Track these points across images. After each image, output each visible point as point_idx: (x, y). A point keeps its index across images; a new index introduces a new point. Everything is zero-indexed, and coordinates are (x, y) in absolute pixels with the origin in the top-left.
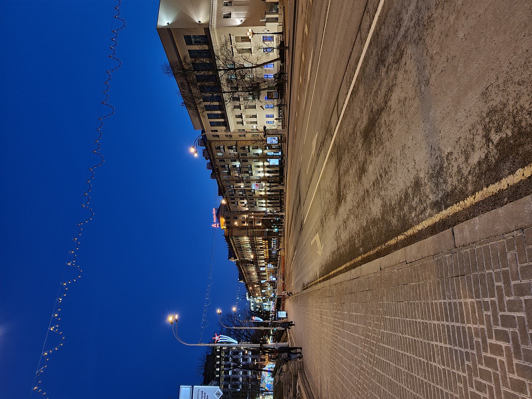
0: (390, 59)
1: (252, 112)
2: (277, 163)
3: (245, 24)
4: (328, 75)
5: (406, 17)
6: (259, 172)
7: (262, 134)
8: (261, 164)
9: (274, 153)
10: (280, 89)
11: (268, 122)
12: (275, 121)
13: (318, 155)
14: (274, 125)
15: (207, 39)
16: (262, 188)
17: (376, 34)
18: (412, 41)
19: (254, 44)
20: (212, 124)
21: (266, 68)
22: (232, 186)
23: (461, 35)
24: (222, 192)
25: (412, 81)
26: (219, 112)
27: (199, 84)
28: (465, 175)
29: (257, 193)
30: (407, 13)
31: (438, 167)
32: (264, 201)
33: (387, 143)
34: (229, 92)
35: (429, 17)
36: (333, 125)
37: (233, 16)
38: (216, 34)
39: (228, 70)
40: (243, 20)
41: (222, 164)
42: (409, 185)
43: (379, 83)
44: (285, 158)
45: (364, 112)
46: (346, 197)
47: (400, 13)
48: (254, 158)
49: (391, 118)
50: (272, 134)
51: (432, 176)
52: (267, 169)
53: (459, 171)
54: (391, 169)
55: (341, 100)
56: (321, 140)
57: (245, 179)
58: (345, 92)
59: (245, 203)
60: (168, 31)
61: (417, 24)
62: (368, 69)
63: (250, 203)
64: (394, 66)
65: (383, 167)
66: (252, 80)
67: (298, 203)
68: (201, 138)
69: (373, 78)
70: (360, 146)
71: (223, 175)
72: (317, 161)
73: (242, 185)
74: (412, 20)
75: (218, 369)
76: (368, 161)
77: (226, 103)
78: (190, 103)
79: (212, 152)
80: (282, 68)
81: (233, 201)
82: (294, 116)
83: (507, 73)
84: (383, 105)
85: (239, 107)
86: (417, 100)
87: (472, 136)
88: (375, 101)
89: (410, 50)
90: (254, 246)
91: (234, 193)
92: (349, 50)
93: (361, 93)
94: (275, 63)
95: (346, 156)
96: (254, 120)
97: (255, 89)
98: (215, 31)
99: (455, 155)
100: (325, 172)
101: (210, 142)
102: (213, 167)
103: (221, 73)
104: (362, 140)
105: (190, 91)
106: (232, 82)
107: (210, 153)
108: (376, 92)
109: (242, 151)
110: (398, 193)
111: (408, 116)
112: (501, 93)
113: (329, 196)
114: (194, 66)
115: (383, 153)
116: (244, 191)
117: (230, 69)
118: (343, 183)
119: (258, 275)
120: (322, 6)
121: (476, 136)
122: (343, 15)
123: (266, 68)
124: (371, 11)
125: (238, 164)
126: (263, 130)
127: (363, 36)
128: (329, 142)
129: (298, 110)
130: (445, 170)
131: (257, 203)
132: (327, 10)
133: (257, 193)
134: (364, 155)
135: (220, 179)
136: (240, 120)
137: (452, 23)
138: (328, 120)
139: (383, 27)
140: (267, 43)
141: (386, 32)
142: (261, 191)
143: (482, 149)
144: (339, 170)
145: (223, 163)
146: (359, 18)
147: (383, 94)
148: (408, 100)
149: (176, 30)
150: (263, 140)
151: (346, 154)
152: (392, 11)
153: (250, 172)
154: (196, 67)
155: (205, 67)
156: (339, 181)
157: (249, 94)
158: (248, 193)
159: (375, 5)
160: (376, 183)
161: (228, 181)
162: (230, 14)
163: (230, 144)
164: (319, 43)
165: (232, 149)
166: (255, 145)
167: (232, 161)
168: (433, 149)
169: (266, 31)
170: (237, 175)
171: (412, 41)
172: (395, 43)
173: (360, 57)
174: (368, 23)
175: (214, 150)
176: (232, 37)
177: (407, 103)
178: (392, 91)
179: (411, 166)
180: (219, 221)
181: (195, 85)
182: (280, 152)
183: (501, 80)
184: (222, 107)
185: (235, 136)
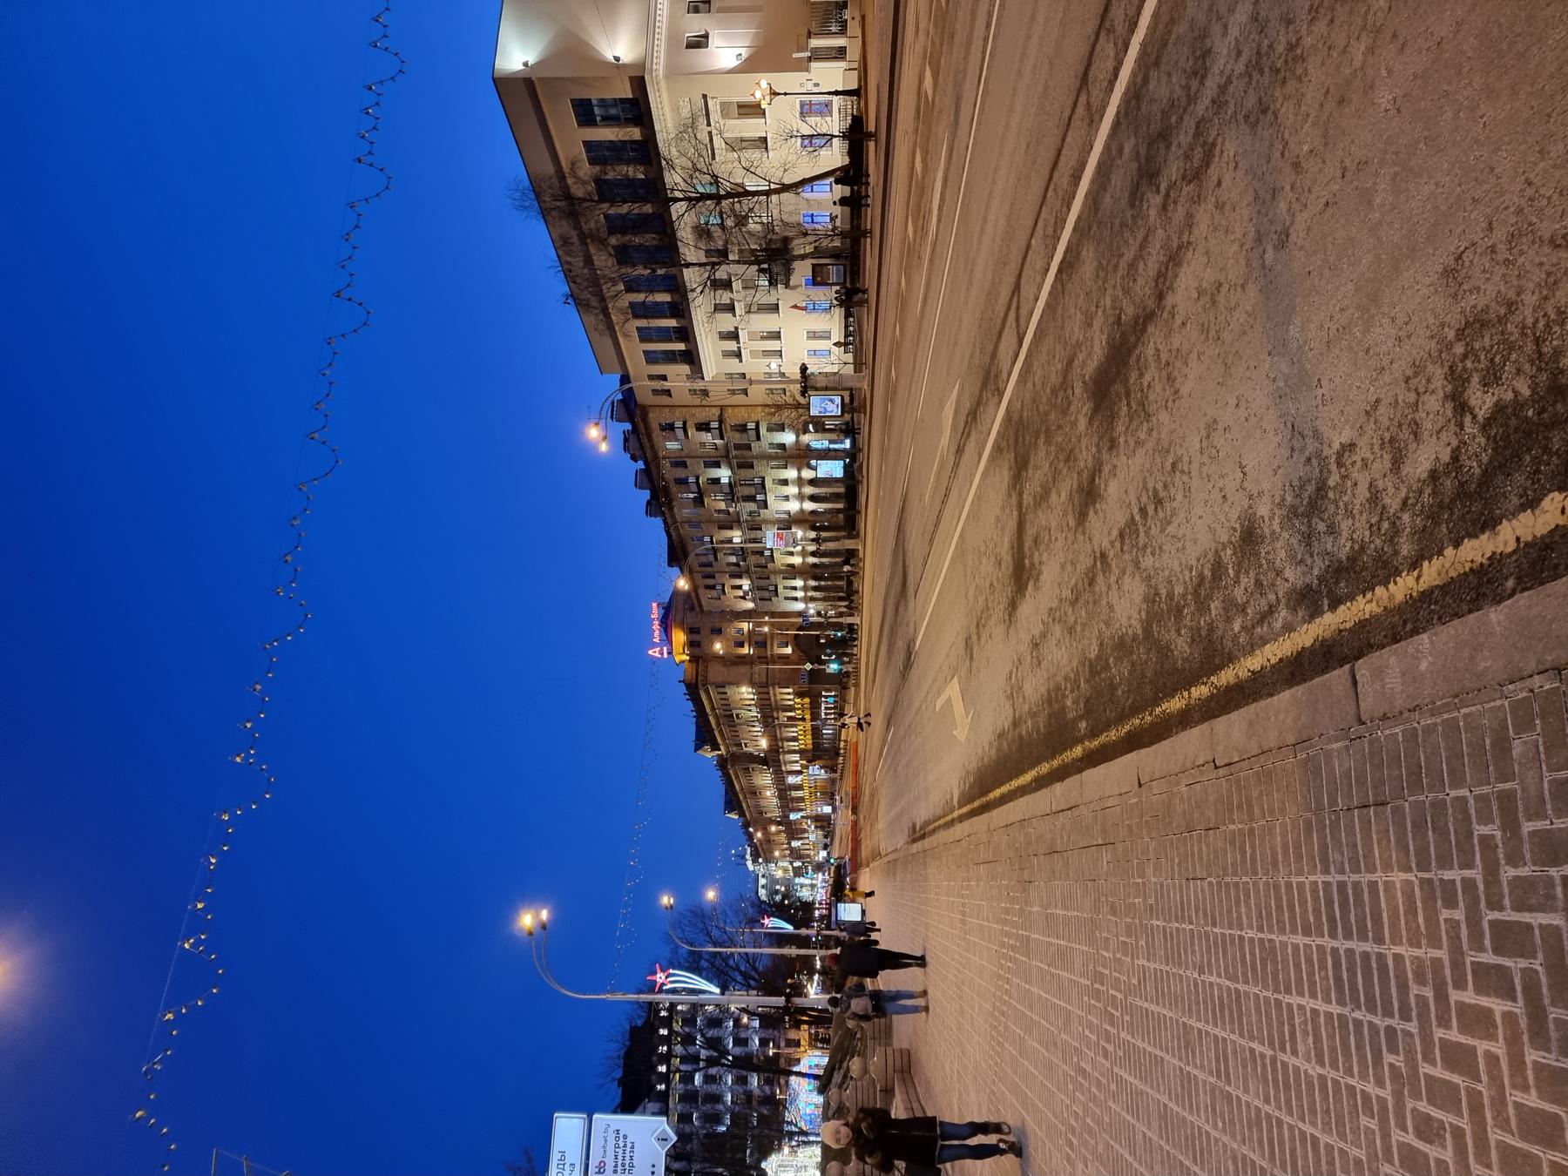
0: (1173, 170)
1: (767, 322)
4: (991, 217)
5: (1222, 48)
6: (787, 498)
8: (791, 474)
9: (831, 442)
10: (847, 268)
12: (835, 349)
13: (960, 451)
14: (831, 360)
15: (637, 110)
16: (795, 544)
20: (651, 358)
22: (707, 539)
23: (1384, 98)
26: (672, 323)
27: (613, 241)
28: (1392, 511)
29: (781, 560)
31: (1311, 488)
32: (799, 583)
33: (1164, 417)
34: (701, 265)
35: (1291, 47)
37: (715, 41)
39: (698, 200)
40: (745, 53)
41: (680, 473)
47: (1204, 35)
48: (770, 457)
50: (826, 389)
52: (809, 490)
54: (1173, 491)
55: (1027, 290)
58: (1039, 265)
59: (746, 588)
61: (1256, 65)
62: (1107, 199)
63: (761, 589)
65: (1150, 486)
66: (769, 228)
68: (620, 397)
69: (1123, 225)
70: (1082, 423)
71: (682, 506)
72: (956, 465)
74: (1239, 53)
76: (1106, 469)
77: (691, 296)
78: (588, 295)
81: (710, 582)
83: (1519, 211)
84: (1151, 304)
85: (730, 308)
87: (1412, 397)
88: (1127, 291)
89: (1231, 144)
91: (711, 558)
92: (1051, 142)
93: (1087, 268)
95: (1042, 453)
96: (773, 345)
97: (774, 257)
99: (1363, 452)
100: (978, 497)
101: (645, 410)
103: (677, 209)
104: (1089, 406)
105: (588, 260)
108: (1132, 266)
109: (737, 438)
110: (1194, 563)
115: (1151, 445)
116: (742, 553)
117: (704, 197)
118: (1030, 532)
121: (1426, 397)
124: (1120, 28)
125: (724, 474)
126: (798, 376)
128: (991, 409)
129: (902, 318)
130: (1331, 495)
133: (781, 560)
135: (673, 516)
136: (732, 345)
137: (1357, 64)
138: (990, 348)
139: (1154, 74)
140: (812, 120)
141: (1161, 89)
142: (791, 554)
143: (1443, 435)
144: (1020, 495)
145: (680, 474)
146: (1084, 49)
147: (1152, 273)
148: (1225, 289)
150: (798, 406)
152: (1181, 29)
153: (759, 497)
154: (606, 191)
157: (761, 271)
158: (752, 560)
160: (1128, 532)
162: (706, 36)
164: (962, 132)
166: (776, 419)
169: (810, 87)
170: (722, 506)
172: (1189, 124)
174: (1110, 64)
175: (657, 434)
177: (1221, 299)
178: (1179, 264)
179: (1232, 481)
181: (602, 243)
183: (1500, 234)
184: (680, 309)
185: (718, 395)
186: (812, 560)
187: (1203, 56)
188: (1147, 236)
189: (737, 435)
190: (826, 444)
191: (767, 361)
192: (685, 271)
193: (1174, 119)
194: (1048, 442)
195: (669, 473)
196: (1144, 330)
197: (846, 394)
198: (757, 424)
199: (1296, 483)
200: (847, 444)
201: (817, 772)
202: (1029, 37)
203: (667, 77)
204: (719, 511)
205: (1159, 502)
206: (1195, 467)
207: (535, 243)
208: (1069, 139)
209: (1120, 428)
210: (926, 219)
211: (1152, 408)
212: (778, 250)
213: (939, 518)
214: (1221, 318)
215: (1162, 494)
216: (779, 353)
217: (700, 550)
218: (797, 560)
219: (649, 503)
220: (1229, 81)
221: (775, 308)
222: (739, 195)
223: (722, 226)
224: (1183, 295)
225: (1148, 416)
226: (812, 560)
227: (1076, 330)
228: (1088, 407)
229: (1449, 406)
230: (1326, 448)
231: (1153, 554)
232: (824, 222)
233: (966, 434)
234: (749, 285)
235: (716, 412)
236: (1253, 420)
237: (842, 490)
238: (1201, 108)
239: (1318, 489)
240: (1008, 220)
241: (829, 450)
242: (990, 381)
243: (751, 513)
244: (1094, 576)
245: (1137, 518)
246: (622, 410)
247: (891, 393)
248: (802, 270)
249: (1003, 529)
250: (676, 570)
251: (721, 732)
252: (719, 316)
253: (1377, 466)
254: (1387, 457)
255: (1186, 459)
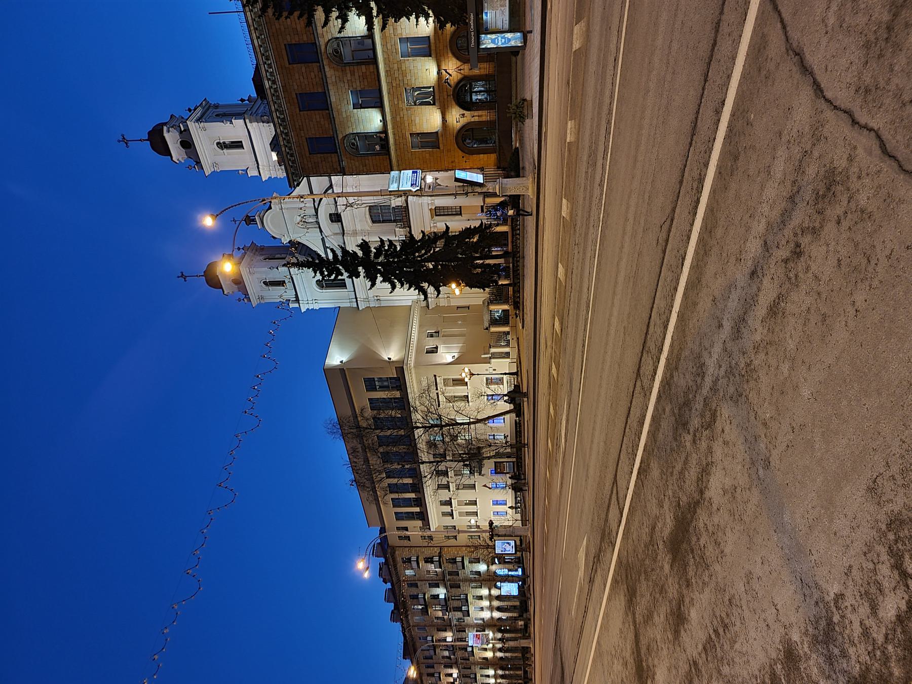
0: (695, 422)
1: (468, 495)
2: (515, 592)
4: (596, 441)
5: (711, 364)
6: (482, 609)
7: (486, 535)
8: (484, 592)
9: (509, 570)
10: (516, 464)
11: (497, 513)
12: (510, 511)
13: (591, 581)
14: (508, 517)
15: (399, 382)
16: (488, 643)
17: (667, 383)
18: (728, 397)
20: (399, 517)
21: (491, 425)
22: (429, 638)
23: (806, 392)
24: (409, 651)
25: (741, 460)
26: (412, 495)
27: (381, 450)
28: (880, 643)
29: (479, 654)
30: (711, 357)
31: (823, 623)
32: (491, 672)
33: (717, 567)
34: (430, 462)
35: (748, 365)
36: (614, 526)
37: (440, 350)
38: (414, 375)
39: (430, 427)
40: (456, 355)
41: (414, 591)
42: (774, 655)
43: (683, 459)
44: (529, 581)
45: (666, 507)
46: (654, 674)
47: (699, 356)
48: (471, 581)
49: (716, 520)
50: (505, 536)
51: (815, 641)
52: (496, 603)
53: (866, 633)
54: (733, 619)
55: (621, 483)
56: (593, 551)
57: (455, 622)
58: (626, 469)
59: (455, 675)
60: (341, 371)
61: (730, 372)
62: (660, 435)
63: (465, 676)
64: (705, 433)
65: (718, 614)
66: (469, 442)
67: (559, 679)
68: (379, 541)
69: (672, 450)
70: (667, 567)
71: (414, 614)
72: (590, 591)
73: (449, 636)
74: (720, 366)
76: (687, 600)
77: (424, 480)
78: (365, 481)
79: (396, 569)
80: (518, 428)
81: (431, 671)
82: (542, 504)
83: (902, 457)
84: (696, 496)
85: (447, 487)
86: (756, 492)
87: (871, 566)
88: (681, 488)
89: (725, 411)
91: (432, 652)
92: (624, 404)
93: (655, 472)
94: (507, 417)
95: (644, 587)
96: (471, 508)
97: (473, 457)
98: (413, 371)
99: (849, 601)
100: (606, 615)
101: (393, 549)
102: (395, 597)
103: (418, 432)
104: (669, 556)
105: (366, 460)
106: (435, 446)
107: (392, 569)
108: (681, 473)
109: (450, 567)
110: (757, 673)
111: (745, 518)
112: (901, 491)
113: (620, 668)
114: (376, 422)
115: (712, 585)
116: (452, 649)
117: (433, 426)
118: (644, 642)
120: (575, 340)
121: (880, 566)
122: (609, 353)
123: (491, 425)
124: (654, 351)
125: (441, 592)
126: (488, 528)
127: (646, 385)
128: (608, 555)
129: (548, 495)
130: (837, 628)
132: (584, 346)
133: (479, 654)
134: (677, 586)
135: (408, 622)
136: (447, 509)
137: (787, 375)
138: (603, 516)
139: (675, 374)
140: (493, 387)
141: (682, 381)
142: (486, 650)
143: (898, 592)
144: (634, 614)
145: (416, 591)
146: (637, 360)
147: (694, 478)
148: (739, 490)
150: (488, 547)
151: (644, 582)
152: (686, 353)
153: (464, 608)
154: (378, 423)
155: (394, 423)
156: (636, 637)
157: (465, 465)
158: (460, 654)
159: (659, 344)
160: (709, 646)
161: (422, 627)
162: (437, 348)
163: (428, 553)
164: (575, 392)
165: (432, 562)
166: (474, 555)
168: (807, 586)
169: (491, 370)
170: (440, 614)
171: (728, 397)
172: (700, 399)
173: (645, 416)
174: (651, 368)
176: (438, 379)
177: (738, 495)
178: (709, 474)
179: (770, 614)
181: (375, 451)
182: (520, 570)
183: (895, 469)
184: (418, 488)
185: (439, 539)
186: (499, 654)
187: (701, 372)
188: (686, 459)
189: (450, 565)
190: (506, 572)
191: (469, 518)
192: (421, 466)
193: (691, 396)
194: (647, 579)
195: (406, 591)
196: (695, 512)
197: (518, 539)
199: (812, 619)
200: (520, 572)
202: (606, 352)
203: (415, 367)
204: (437, 618)
205: (726, 627)
206: (744, 603)
207: (338, 451)
208: (634, 403)
209: (691, 573)
210: (558, 439)
211: (709, 561)
212: (475, 454)
213: (582, 628)
214: (740, 508)
215: (727, 621)
216: (476, 514)
217: (425, 647)
218: (489, 654)
219: (392, 612)
220: (717, 379)
221: (473, 487)
222: (453, 425)
223: (443, 441)
224: (714, 489)
225: (707, 567)
226: (499, 654)
227: (654, 508)
228: (668, 558)
229: (896, 572)
230: (826, 596)
231: (729, 665)
232: (500, 437)
233: (594, 570)
234: (458, 474)
235: (437, 550)
236: (775, 574)
237: (518, 603)
238: (705, 391)
239: (828, 624)
240: (605, 443)
241: (508, 576)
242: (605, 537)
243: (459, 619)
244: (692, 679)
245: (713, 636)
247: (545, 540)
248: (489, 465)
249: (625, 638)
250: (408, 661)
252: (440, 491)
253: (861, 610)
254: (867, 604)
255: (737, 597)
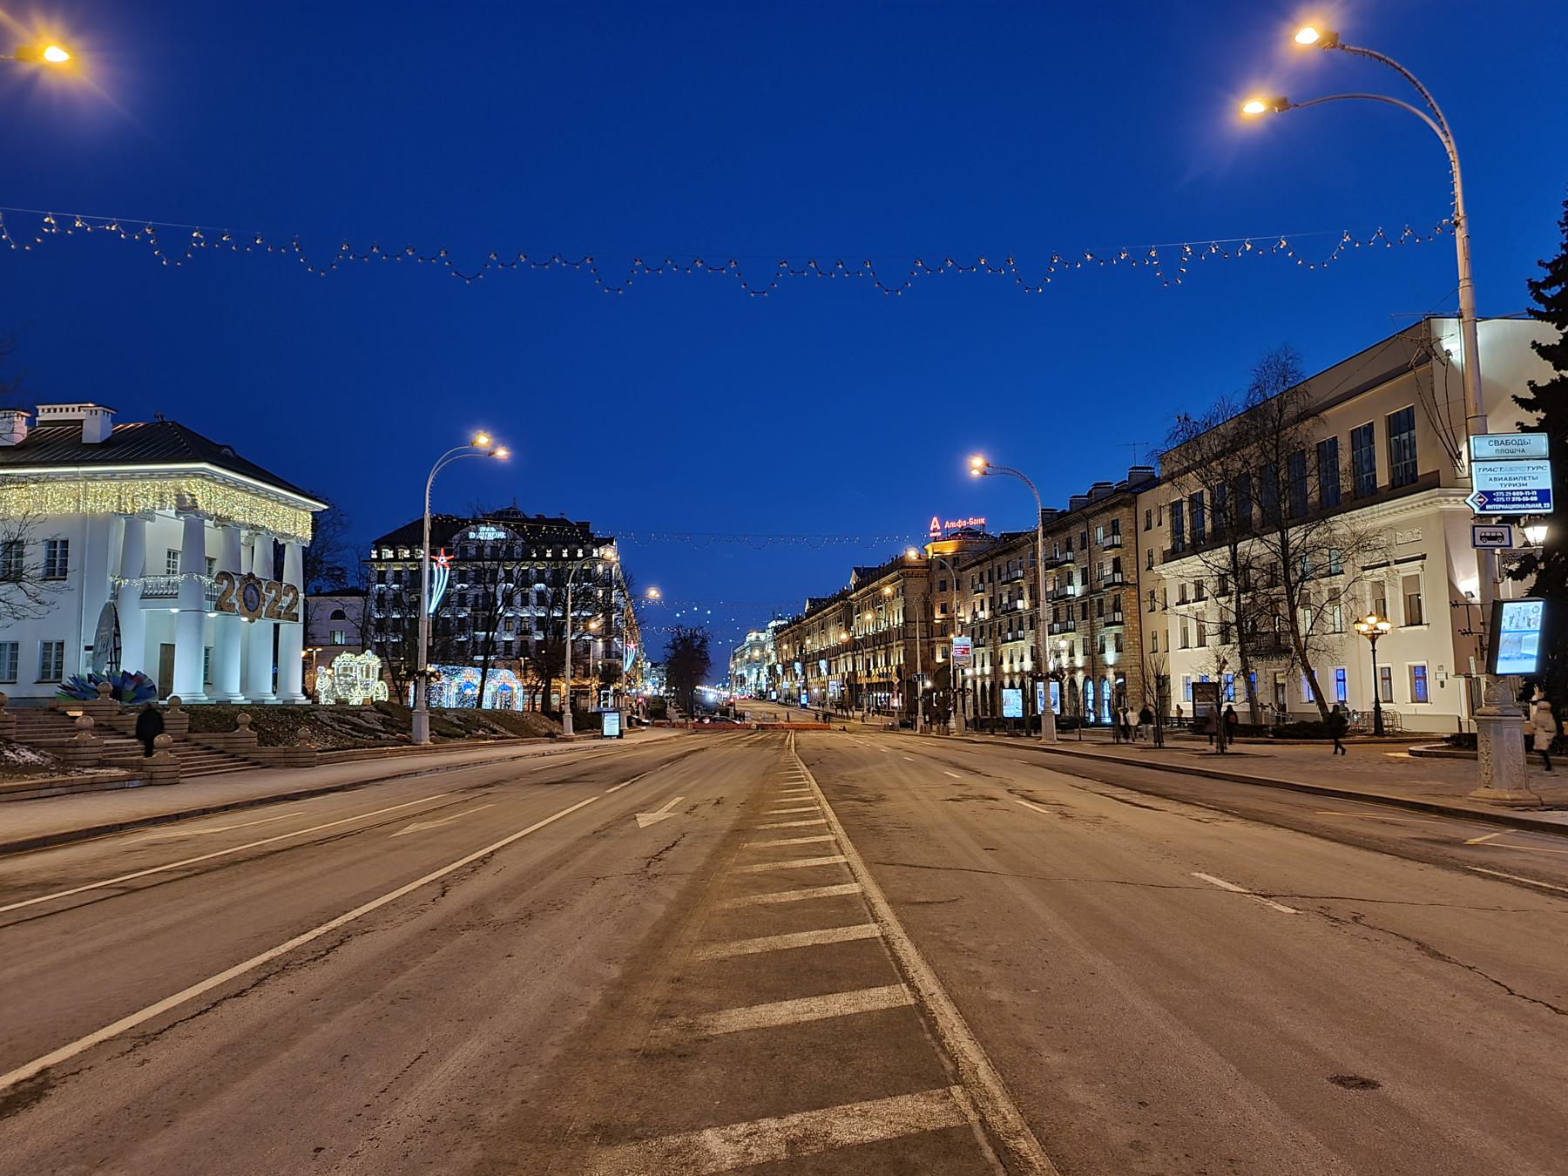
3: (1457, 602)
8: (1079, 661)
15: (1407, 482)
19: (1399, 635)
20: (1176, 508)
29: (1006, 649)
32: (987, 670)
38: (1422, 512)
41: (1076, 544)
60: (1430, 351)
75: (580, 554)
78: (1191, 445)
90: (881, 640)
91: (1004, 578)
98: (1431, 510)
101: (1132, 503)
109: (1109, 602)
119: (821, 652)
131: (982, 650)
133: (1006, 649)
145: (1066, 543)
149: (1424, 389)
153: (1057, 626)
158: (1005, 620)
163: (1127, 563)
167: (1084, 572)
175: (1108, 517)
180: (948, 535)
189: (1111, 602)
195: (1076, 532)
198: (1121, 623)
201: (834, 689)
218: (1006, 667)
235: (1131, 579)
246: (1142, 479)
251: (867, 593)
